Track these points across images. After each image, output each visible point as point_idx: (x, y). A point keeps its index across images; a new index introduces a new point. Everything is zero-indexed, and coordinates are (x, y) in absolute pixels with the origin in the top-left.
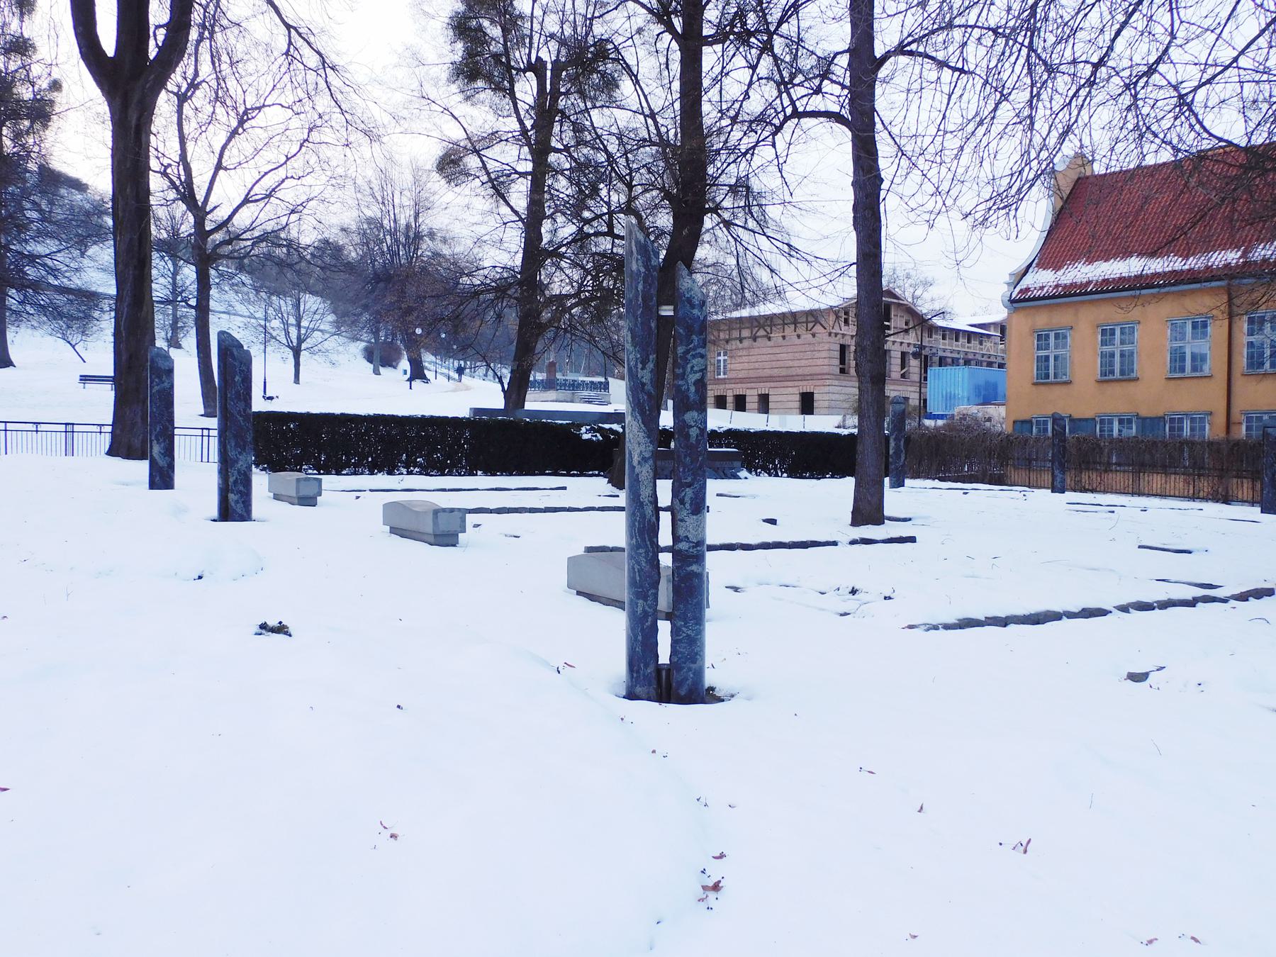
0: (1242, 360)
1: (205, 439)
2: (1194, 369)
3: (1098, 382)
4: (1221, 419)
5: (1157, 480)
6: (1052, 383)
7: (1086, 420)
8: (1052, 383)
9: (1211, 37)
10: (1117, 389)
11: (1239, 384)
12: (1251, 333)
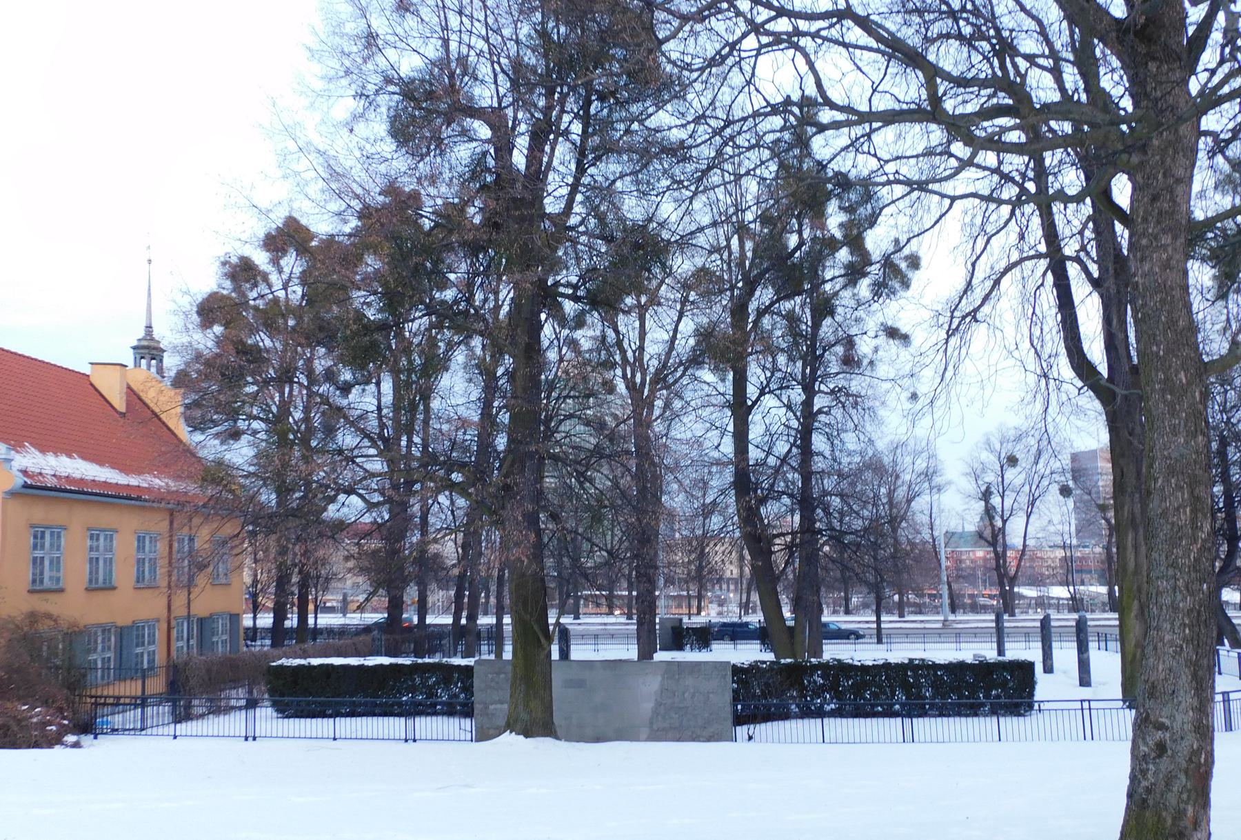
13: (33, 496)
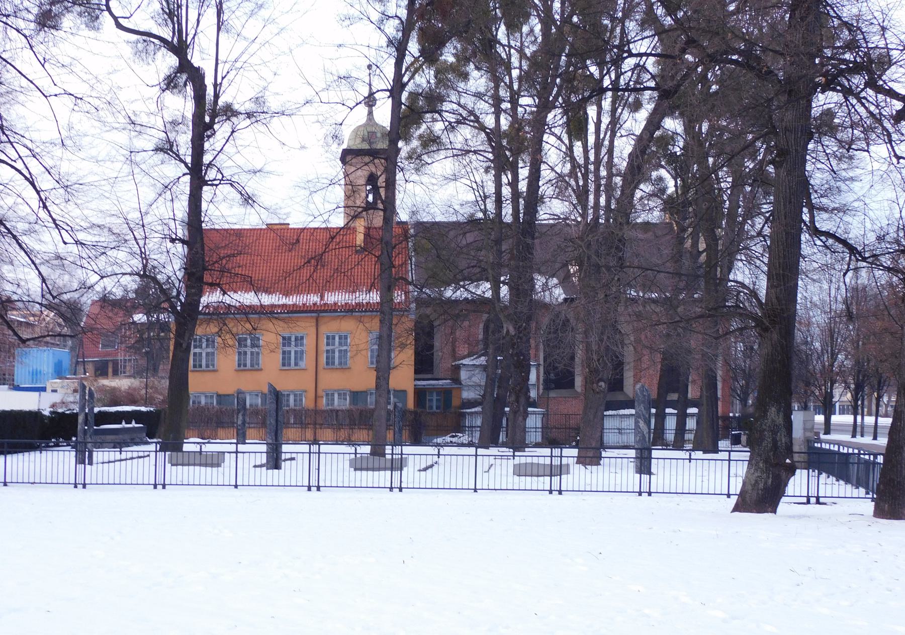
0: (323, 359)
1: (314, 457)
2: (296, 364)
3: (236, 370)
4: (312, 395)
5: (221, 432)
6: (204, 371)
7: (228, 395)
8: (204, 371)
9: (137, 170)
10: (248, 375)
11: (323, 375)
12: (328, 344)
13: (307, 317)
